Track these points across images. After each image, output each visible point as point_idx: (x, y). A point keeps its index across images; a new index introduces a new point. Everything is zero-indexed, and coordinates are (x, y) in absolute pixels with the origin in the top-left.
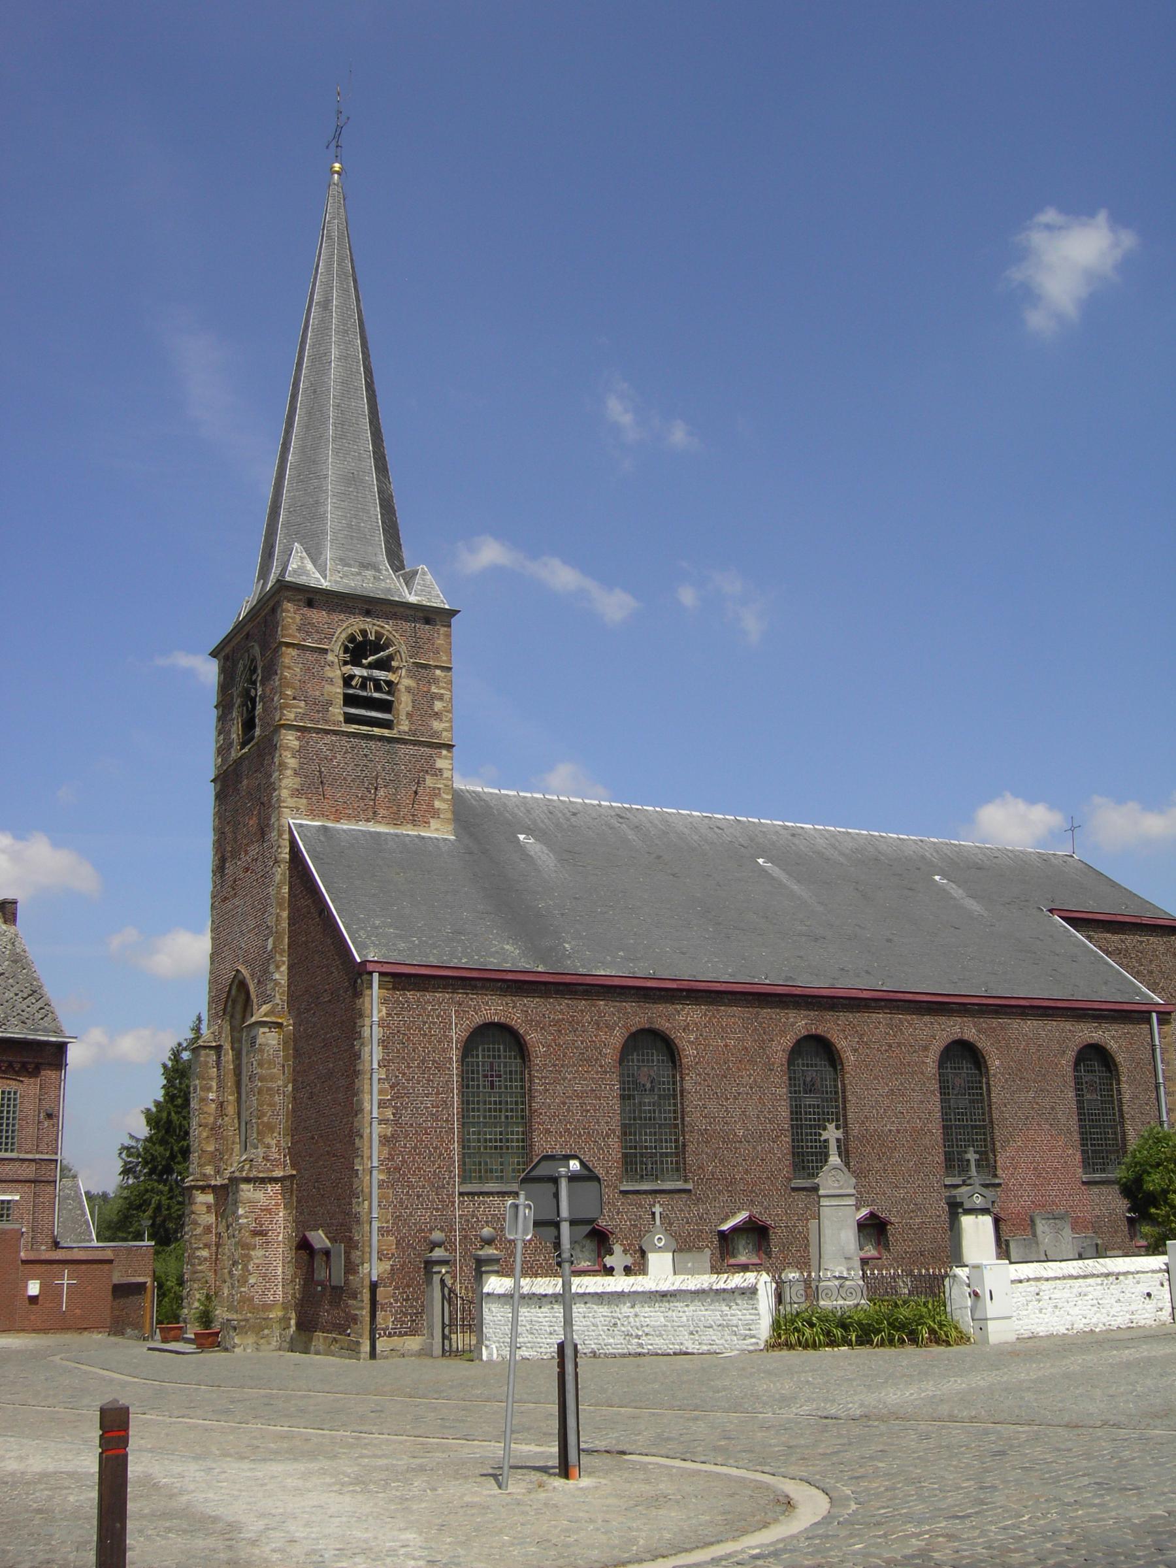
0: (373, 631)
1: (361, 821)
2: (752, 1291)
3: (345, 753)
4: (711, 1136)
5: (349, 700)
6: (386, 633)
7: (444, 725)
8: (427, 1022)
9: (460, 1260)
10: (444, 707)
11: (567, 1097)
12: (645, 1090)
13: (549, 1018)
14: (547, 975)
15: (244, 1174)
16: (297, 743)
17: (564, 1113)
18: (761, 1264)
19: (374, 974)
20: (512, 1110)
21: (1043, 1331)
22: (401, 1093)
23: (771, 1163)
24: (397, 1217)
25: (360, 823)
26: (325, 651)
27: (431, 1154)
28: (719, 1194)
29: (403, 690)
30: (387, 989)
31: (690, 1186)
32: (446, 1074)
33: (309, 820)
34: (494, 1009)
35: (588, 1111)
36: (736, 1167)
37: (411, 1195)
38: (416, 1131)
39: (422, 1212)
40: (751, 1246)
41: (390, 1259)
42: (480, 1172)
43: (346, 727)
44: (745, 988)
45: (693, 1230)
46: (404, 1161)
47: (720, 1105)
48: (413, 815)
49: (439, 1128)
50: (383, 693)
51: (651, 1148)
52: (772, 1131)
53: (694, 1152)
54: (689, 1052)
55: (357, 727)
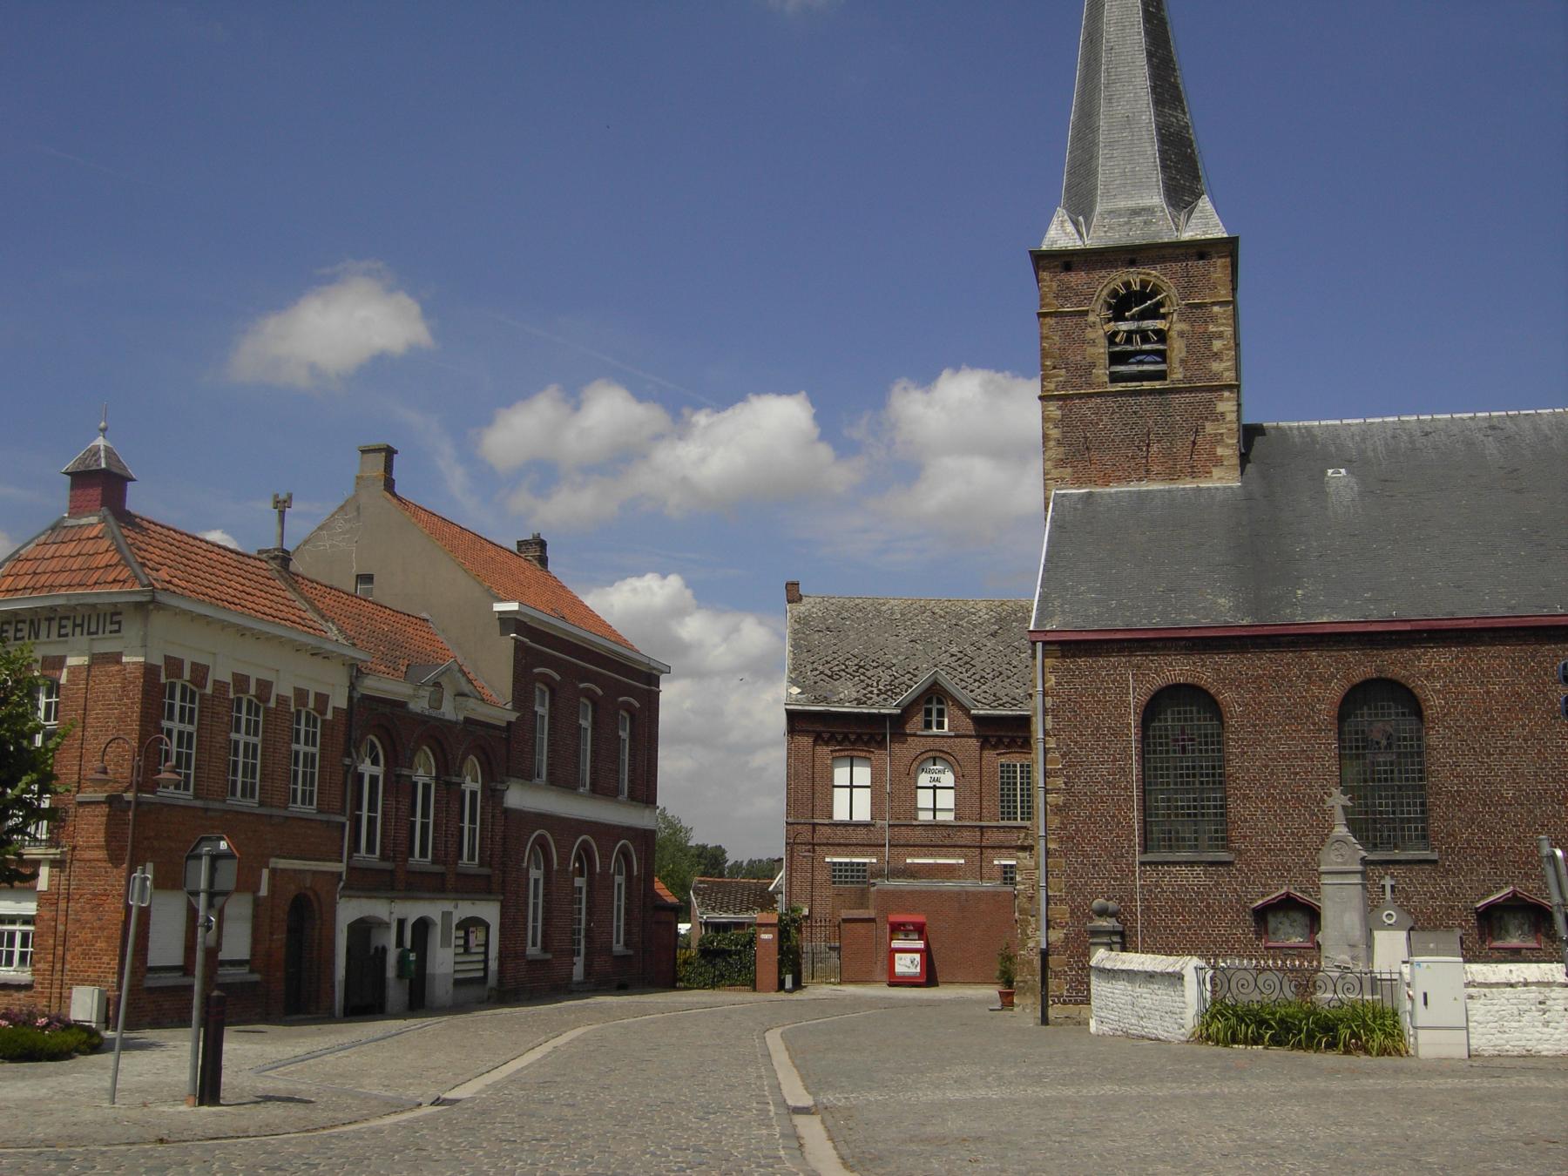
0: (1138, 280)
1: (1133, 481)
2: (1177, 978)
3: (1112, 414)
4: (1466, 800)
5: (1116, 358)
6: (1153, 279)
7: (1225, 364)
8: (1101, 688)
9: (1141, 931)
10: (1224, 345)
11: (1270, 759)
12: (1380, 748)
13: (1247, 674)
14: (1238, 628)
15: (1019, 843)
16: (1059, 412)
17: (1266, 776)
18: (1541, 949)
19: (1038, 643)
20: (1207, 775)
21: (1548, 1050)
22: (1074, 762)
23: (1555, 830)
24: (1071, 885)
25: (1132, 483)
26: (1086, 313)
27: (1107, 823)
28: (1478, 866)
29: (1176, 336)
30: (1056, 658)
31: (1435, 856)
32: (1123, 741)
33: (1075, 489)
34: (1177, 669)
35: (1297, 773)
36: (1502, 834)
37: (1086, 865)
38: (1091, 800)
39: (1098, 882)
40: (1526, 927)
41: (1063, 927)
42: (1170, 840)
43: (1112, 387)
44: (1509, 622)
45: (1440, 906)
46: (1077, 830)
47: (1479, 762)
48: (1192, 467)
49: (1116, 796)
50: (1153, 343)
51: (1387, 813)
52: (1558, 791)
53: (1442, 817)
54: (1434, 704)
55: (1124, 384)
